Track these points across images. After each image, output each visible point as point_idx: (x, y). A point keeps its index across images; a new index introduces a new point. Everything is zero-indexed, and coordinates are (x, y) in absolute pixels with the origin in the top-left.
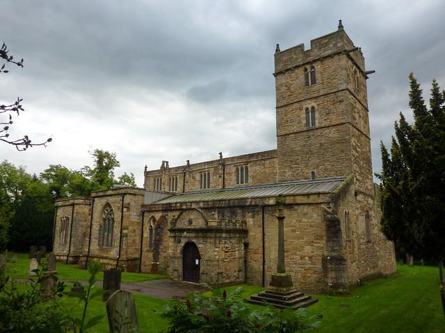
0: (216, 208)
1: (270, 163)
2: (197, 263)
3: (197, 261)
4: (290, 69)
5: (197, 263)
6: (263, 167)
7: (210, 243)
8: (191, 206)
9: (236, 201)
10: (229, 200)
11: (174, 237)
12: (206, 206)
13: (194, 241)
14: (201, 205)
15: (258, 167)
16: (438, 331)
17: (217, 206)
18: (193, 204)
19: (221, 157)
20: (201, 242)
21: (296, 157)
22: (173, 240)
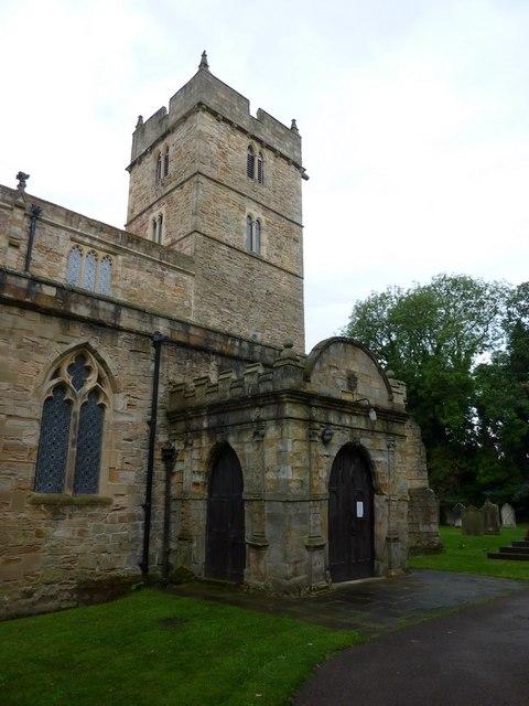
0: (214, 353)
1: (177, 280)
2: (360, 512)
3: (360, 505)
4: (230, 123)
5: (360, 512)
6: (158, 282)
7: (401, 452)
8: (116, 315)
9: (267, 351)
10: (252, 343)
11: (309, 422)
12: (181, 338)
13: (366, 442)
14: (162, 327)
15: (143, 277)
16: (272, 704)
17: (217, 348)
18: (124, 313)
19: (22, 185)
20: (384, 447)
21: (229, 296)
22: (301, 432)
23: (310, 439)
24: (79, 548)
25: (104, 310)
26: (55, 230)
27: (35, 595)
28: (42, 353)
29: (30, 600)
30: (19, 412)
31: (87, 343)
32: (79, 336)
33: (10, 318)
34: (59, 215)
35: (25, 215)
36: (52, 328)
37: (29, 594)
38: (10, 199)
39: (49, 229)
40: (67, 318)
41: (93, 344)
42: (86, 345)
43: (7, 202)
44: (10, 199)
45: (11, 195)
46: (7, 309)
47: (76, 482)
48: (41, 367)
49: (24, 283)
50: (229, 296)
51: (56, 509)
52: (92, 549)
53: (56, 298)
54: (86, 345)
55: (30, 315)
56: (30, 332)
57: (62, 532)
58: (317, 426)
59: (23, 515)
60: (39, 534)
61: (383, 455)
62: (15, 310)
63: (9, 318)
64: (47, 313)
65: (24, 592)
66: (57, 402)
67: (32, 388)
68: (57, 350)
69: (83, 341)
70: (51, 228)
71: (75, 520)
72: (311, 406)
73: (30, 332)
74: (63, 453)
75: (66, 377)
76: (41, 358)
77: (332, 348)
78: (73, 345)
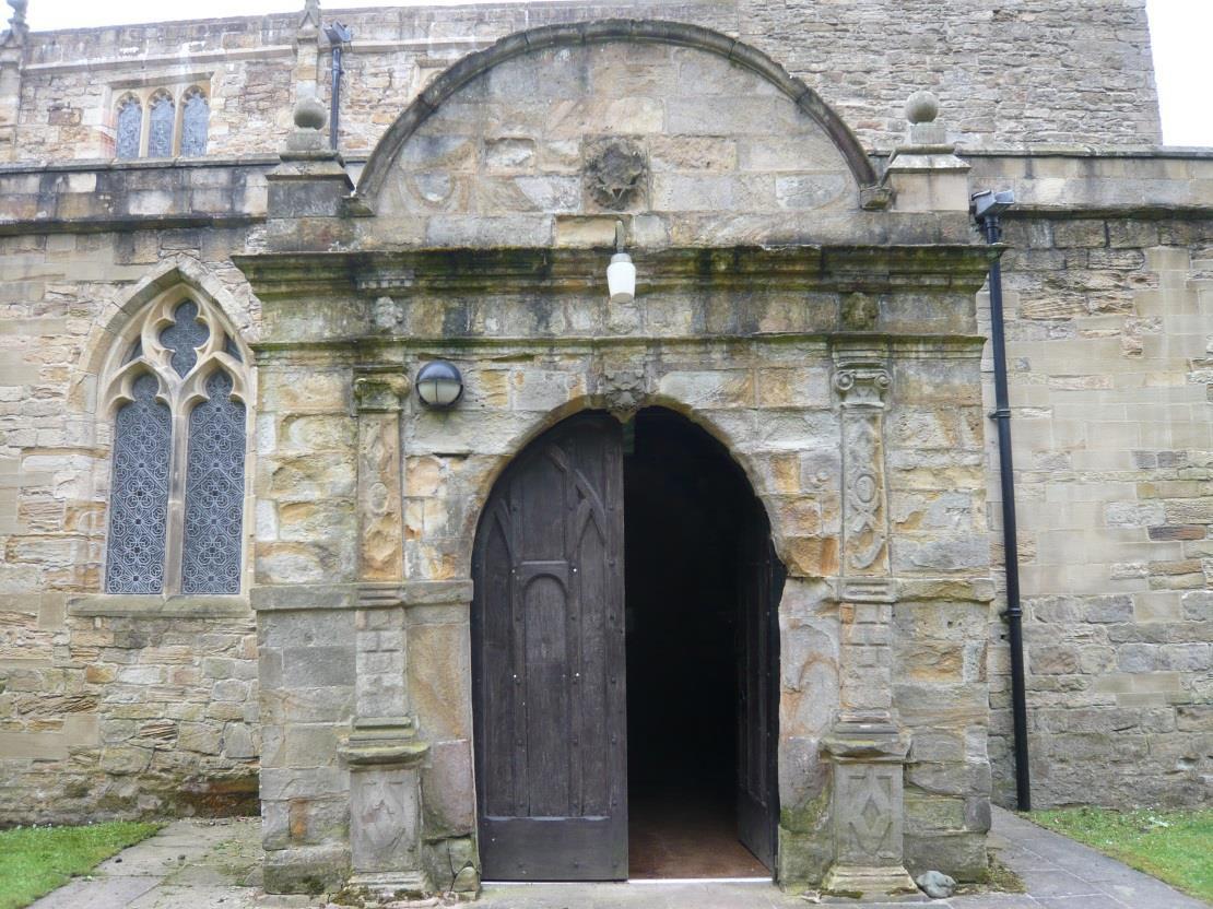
21: (859, 61)
22: (324, 387)
23: (363, 402)
24: (178, 708)
25: (205, 188)
26: (384, 64)
27: (92, 792)
28: (84, 314)
29: (84, 802)
30: (51, 438)
31: (177, 271)
32: (153, 262)
33: (19, 260)
34: (384, 24)
35: (320, 53)
36: (100, 259)
37: (81, 792)
38: (286, 33)
39: (370, 62)
40: (128, 230)
41: (189, 268)
42: (175, 278)
43: (286, 41)
44: (286, 33)
45: (289, 26)
46: (13, 244)
47: (189, 567)
48: (82, 343)
49: (33, 183)
50: (859, 61)
51: (133, 636)
52: (208, 711)
53: (98, 192)
54: (175, 278)
55: (56, 244)
56: (57, 278)
57: (140, 674)
58: (394, 356)
59: (60, 640)
60: (93, 677)
61: (810, 430)
62: (28, 243)
63: (17, 261)
64: (85, 230)
65: (70, 786)
66: (137, 405)
67: (65, 388)
68: (110, 302)
69: (165, 267)
70: (374, 59)
71: (166, 650)
72: (373, 297)
73: (57, 278)
74: (157, 512)
75: (154, 353)
76: (81, 325)
77: (503, 81)
78: (146, 282)
